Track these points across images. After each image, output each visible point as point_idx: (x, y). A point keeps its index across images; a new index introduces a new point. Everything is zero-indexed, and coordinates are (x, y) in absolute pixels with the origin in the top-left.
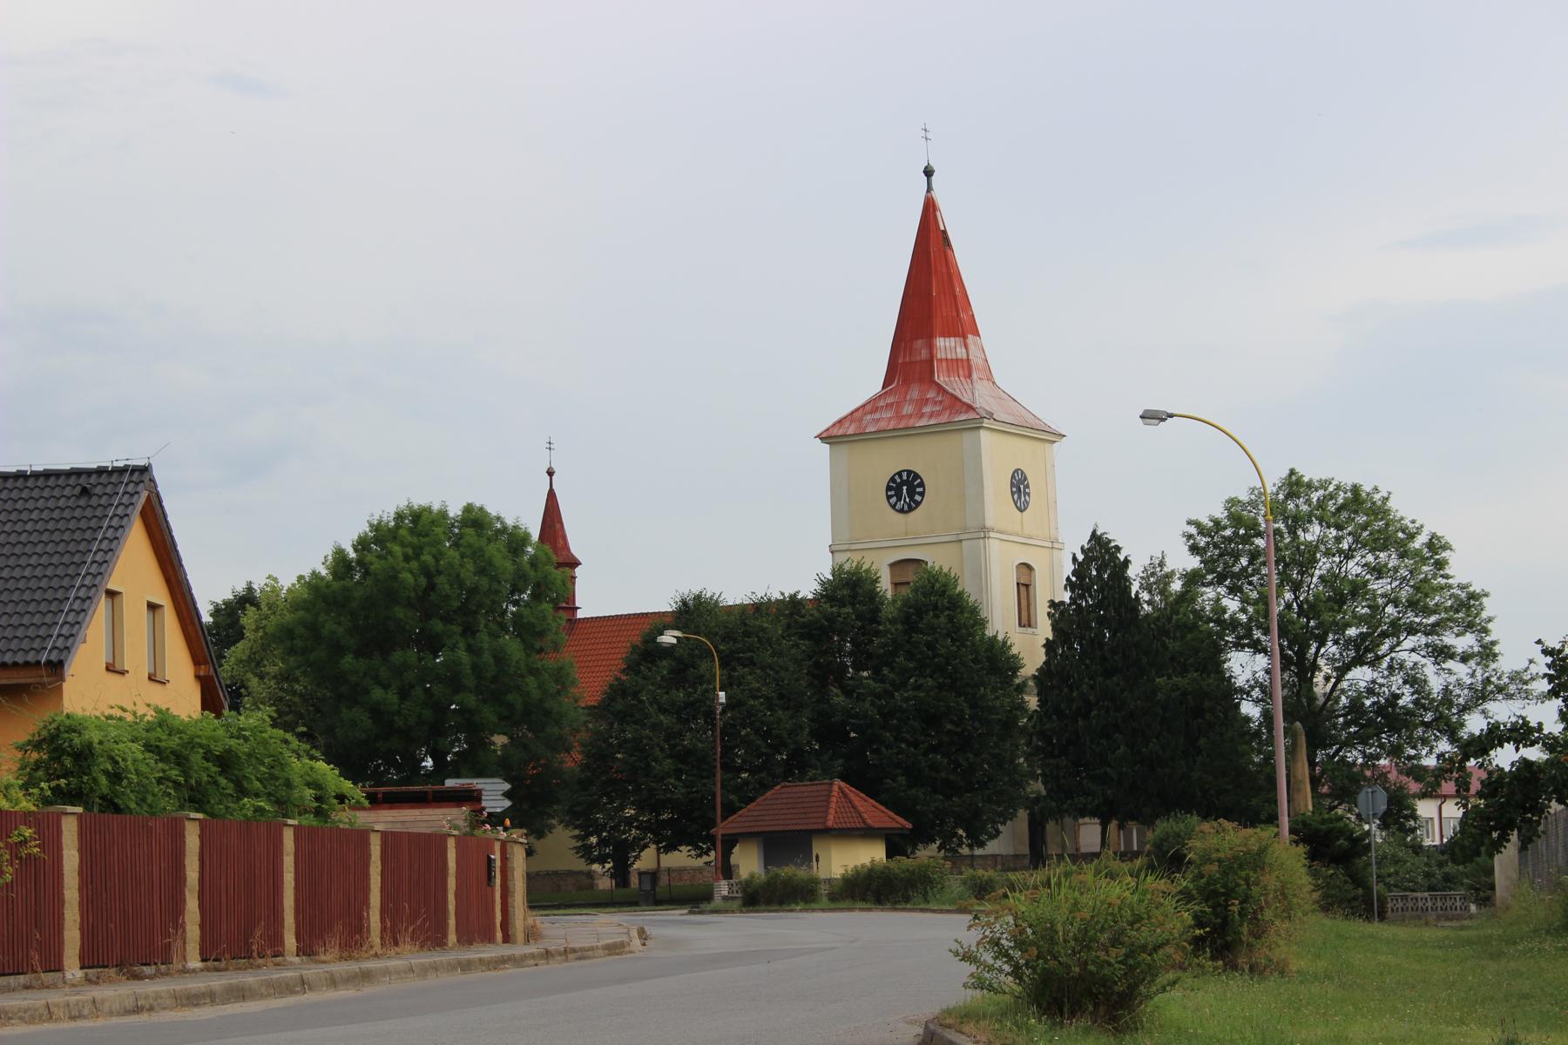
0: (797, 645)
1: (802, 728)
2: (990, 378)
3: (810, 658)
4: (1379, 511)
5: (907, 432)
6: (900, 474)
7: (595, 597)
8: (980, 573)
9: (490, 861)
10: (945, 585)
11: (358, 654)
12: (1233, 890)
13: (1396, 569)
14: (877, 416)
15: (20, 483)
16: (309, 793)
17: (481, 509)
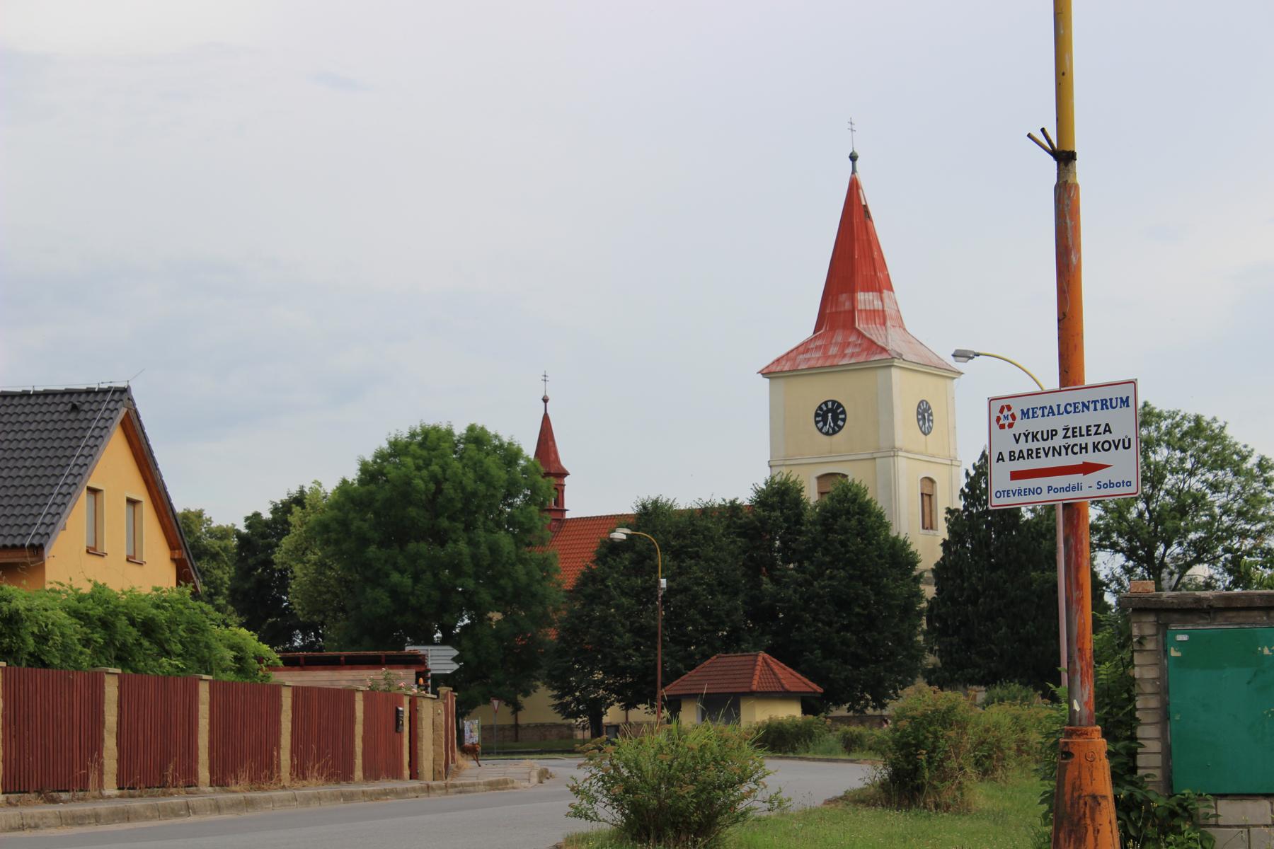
0: (734, 542)
1: (736, 609)
2: (902, 326)
3: (745, 552)
4: (1218, 438)
5: (830, 369)
6: (826, 403)
7: (580, 502)
8: (890, 487)
9: (398, 714)
10: (856, 494)
11: (381, 545)
12: (922, 742)
13: (1230, 485)
14: (808, 356)
15: (24, 401)
16: (229, 654)
17: (482, 428)
